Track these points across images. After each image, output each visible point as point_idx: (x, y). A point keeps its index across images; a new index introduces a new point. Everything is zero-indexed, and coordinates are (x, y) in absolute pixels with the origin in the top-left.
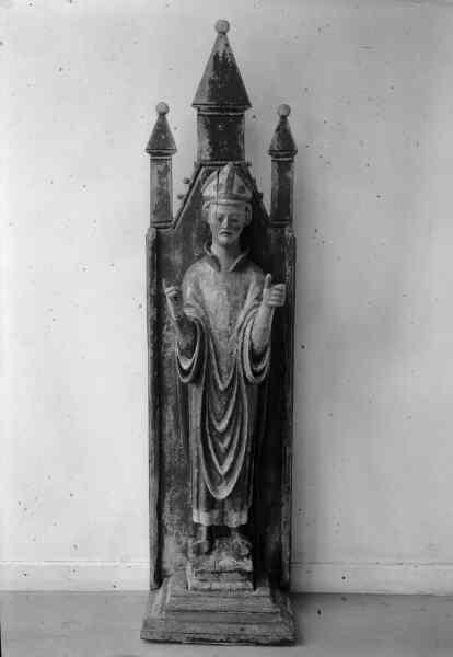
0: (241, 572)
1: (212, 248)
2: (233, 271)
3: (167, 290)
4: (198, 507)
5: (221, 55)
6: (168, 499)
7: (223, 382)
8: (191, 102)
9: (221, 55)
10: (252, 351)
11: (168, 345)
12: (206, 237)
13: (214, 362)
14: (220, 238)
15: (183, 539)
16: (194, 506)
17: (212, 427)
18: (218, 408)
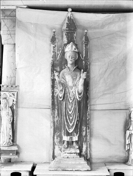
0: (76, 154)
1: (68, 65)
2: (73, 71)
3: (55, 74)
4: (64, 136)
5: (69, 17)
6: (56, 135)
7: (71, 100)
8: (20, 87)
9: (69, 17)
10: (78, 92)
11: (56, 93)
12: (67, 63)
13: (68, 95)
14: (70, 62)
15: (60, 146)
16: (63, 136)
17: (68, 113)
18: (70, 107)
